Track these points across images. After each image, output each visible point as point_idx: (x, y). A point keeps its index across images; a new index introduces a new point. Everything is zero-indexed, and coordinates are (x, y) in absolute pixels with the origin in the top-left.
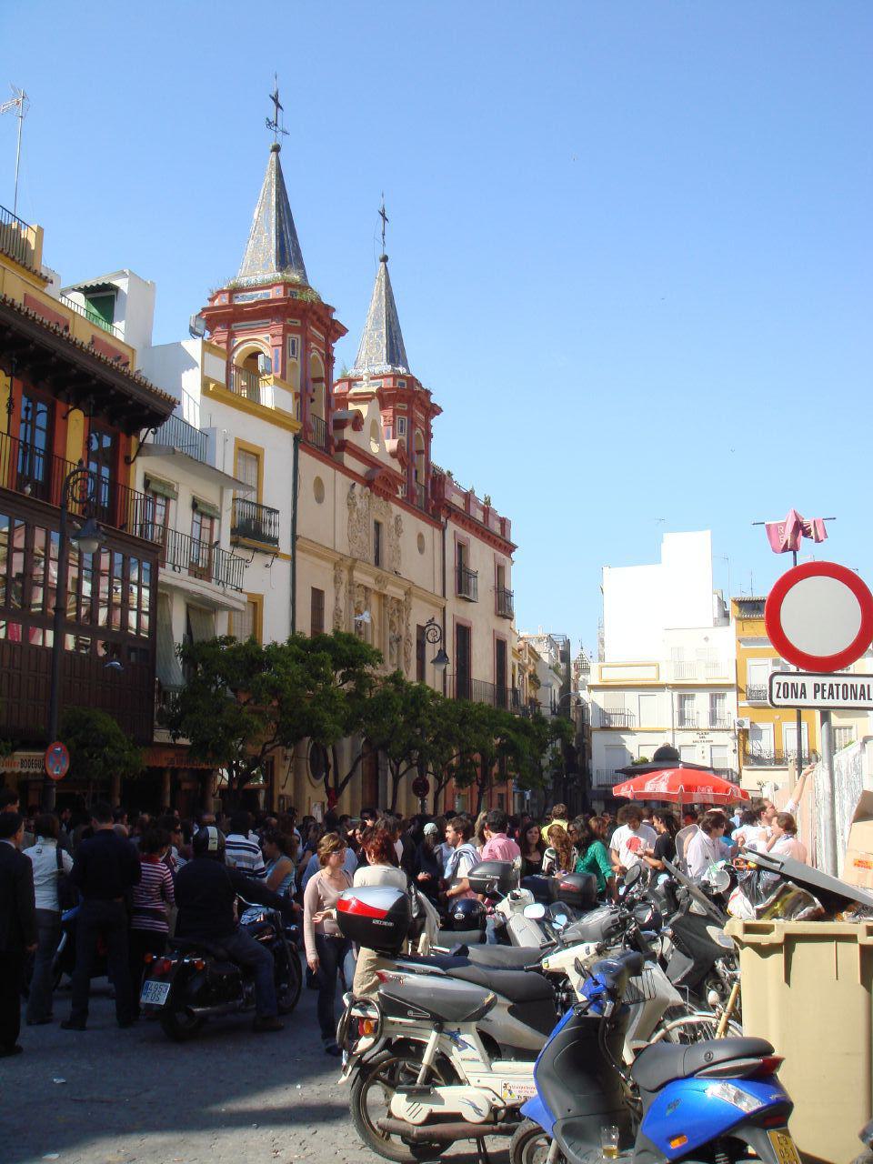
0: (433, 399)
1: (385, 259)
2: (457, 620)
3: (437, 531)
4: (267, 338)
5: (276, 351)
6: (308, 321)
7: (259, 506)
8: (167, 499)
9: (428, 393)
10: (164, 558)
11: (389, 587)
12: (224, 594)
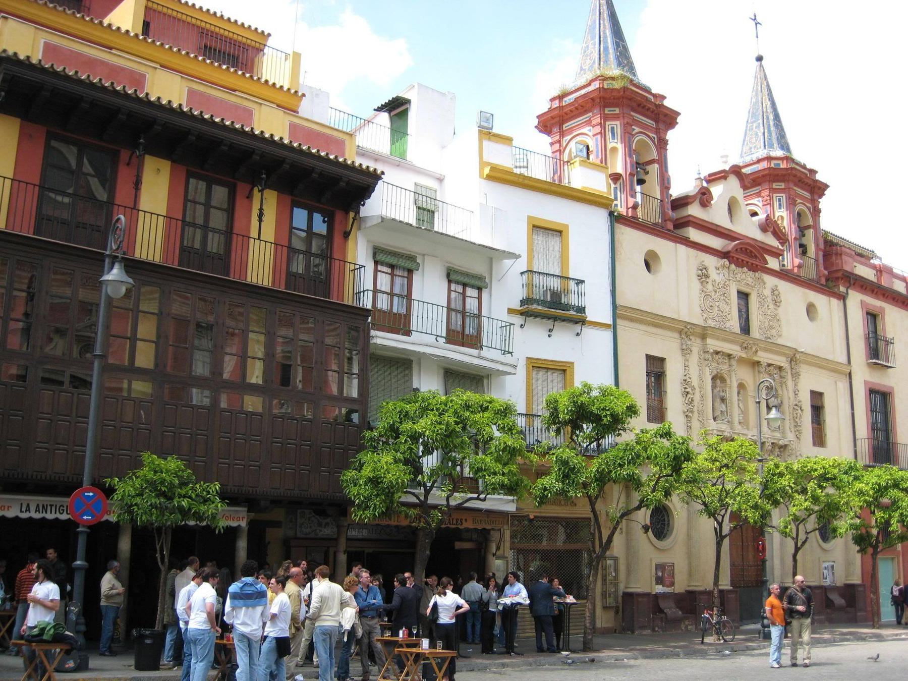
0: (818, 177)
1: (760, 59)
2: (870, 386)
3: (834, 302)
4: (590, 130)
5: (597, 140)
6: (633, 110)
7: (565, 278)
8: (480, 289)
9: (813, 172)
10: (480, 342)
11: (760, 353)
12: (480, 357)
